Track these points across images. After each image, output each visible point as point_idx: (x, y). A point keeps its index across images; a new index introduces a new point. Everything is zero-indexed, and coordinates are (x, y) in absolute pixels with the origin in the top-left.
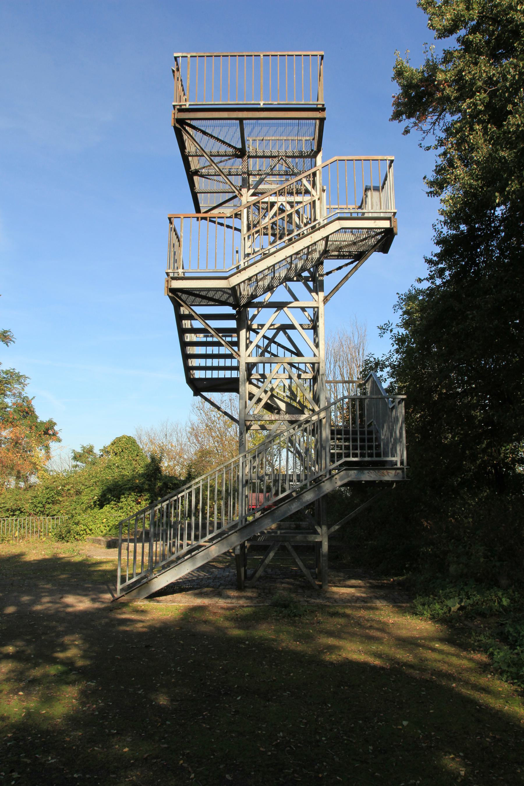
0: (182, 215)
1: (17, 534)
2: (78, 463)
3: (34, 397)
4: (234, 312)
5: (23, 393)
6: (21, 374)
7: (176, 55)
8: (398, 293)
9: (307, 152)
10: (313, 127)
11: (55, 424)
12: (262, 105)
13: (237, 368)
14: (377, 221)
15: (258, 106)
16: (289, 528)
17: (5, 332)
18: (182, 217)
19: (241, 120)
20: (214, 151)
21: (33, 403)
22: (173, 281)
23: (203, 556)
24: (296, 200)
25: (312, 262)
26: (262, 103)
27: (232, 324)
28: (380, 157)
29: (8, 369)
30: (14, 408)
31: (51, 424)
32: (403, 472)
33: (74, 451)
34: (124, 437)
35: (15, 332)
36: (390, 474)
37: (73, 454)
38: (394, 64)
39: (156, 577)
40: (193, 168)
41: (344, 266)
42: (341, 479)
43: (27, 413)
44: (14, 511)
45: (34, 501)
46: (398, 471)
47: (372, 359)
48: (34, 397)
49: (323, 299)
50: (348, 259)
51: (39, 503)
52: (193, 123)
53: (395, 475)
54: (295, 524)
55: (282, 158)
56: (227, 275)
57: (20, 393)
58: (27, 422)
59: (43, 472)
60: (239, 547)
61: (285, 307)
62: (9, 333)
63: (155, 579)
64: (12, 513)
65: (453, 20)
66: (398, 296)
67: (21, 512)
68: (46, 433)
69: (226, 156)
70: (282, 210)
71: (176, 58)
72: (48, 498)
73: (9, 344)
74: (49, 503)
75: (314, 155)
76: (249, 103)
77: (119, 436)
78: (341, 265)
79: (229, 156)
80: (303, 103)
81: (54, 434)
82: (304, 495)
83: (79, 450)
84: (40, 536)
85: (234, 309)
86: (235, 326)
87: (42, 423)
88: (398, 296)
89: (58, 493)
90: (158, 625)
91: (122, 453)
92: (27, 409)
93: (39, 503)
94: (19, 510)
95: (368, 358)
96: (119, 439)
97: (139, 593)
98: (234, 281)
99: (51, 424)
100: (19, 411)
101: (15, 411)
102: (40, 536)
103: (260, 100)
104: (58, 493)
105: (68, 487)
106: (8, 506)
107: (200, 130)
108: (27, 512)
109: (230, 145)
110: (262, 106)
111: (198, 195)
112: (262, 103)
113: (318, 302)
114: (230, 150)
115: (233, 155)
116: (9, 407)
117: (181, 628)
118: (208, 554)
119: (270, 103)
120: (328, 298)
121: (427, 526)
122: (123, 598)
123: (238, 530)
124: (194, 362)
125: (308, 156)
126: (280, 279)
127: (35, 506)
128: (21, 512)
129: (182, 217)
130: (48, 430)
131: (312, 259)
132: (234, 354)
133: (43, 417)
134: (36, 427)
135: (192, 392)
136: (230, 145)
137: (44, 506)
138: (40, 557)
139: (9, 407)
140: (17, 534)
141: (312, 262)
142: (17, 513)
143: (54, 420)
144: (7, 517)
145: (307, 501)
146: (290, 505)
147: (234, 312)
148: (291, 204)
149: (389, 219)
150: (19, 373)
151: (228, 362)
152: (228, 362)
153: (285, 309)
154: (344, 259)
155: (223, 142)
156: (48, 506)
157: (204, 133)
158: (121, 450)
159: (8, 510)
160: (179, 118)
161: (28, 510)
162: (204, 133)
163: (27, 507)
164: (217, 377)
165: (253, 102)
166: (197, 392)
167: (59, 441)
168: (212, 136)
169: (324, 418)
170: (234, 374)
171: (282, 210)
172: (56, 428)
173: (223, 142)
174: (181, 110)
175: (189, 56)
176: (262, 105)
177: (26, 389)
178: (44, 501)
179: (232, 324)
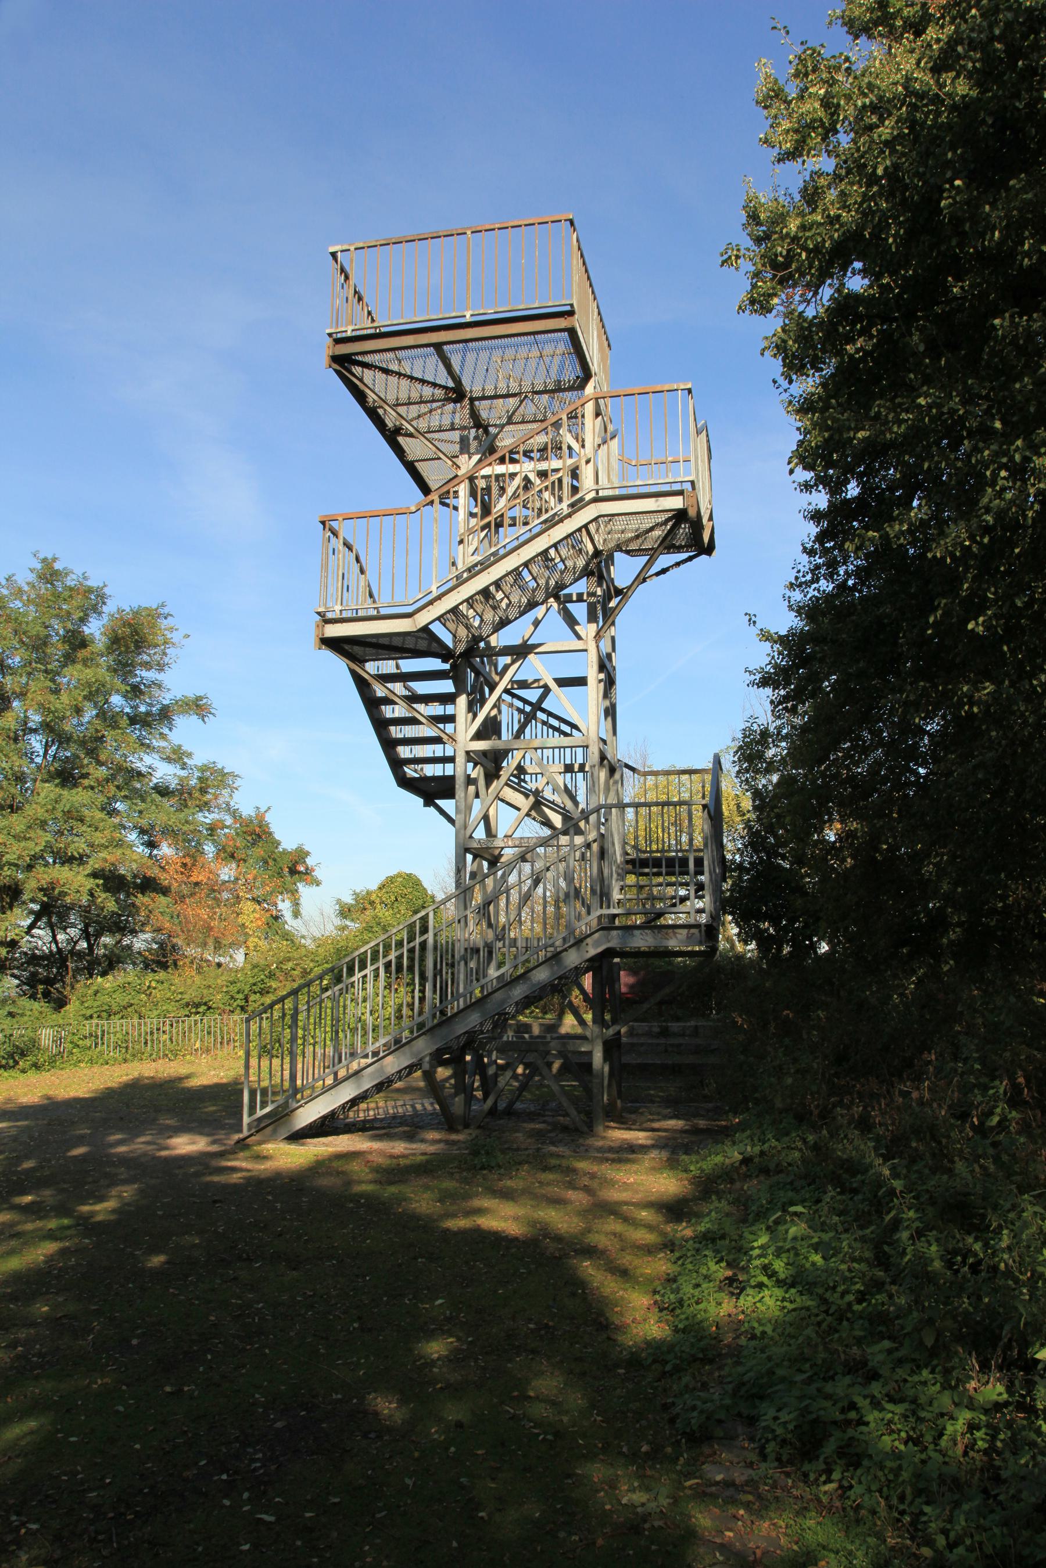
0: (341, 515)
1: (198, 1045)
2: (348, 923)
3: (269, 808)
4: (447, 666)
5: (232, 804)
6: (226, 771)
7: (332, 249)
8: (746, 614)
9: (569, 381)
10: (561, 345)
11: (308, 854)
12: (468, 316)
13: (451, 760)
14: (661, 499)
15: (463, 320)
16: (649, 1034)
17: (199, 698)
18: (340, 519)
19: (438, 347)
20: (403, 397)
21: (268, 818)
22: (327, 626)
23: (372, 1073)
24: (552, 467)
25: (574, 573)
26: (468, 314)
27: (446, 686)
28: (666, 387)
29: (205, 762)
30: (237, 829)
31: (301, 855)
32: (700, 931)
33: (339, 902)
34: (399, 875)
35: (215, 701)
36: (679, 936)
37: (337, 907)
38: (742, 202)
39: (301, 1106)
40: (390, 424)
41: (672, 566)
42: (597, 944)
43: (259, 836)
44: (197, 1006)
45: (231, 988)
46: (693, 931)
47: (755, 726)
48: (269, 808)
49: (594, 634)
50: (687, 551)
51: (238, 992)
52: (368, 359)
53: (688, 937)
54: (659, 1026)
55: (526, 397)
56: (409, 610)
57: (228, 804)
58: (259, 851)
59: (256, 940)
60: (427, 1059)
61: (530, 653)
62: (205, 701)
63: (301, 1110)
64: (194, 1010)
65: (796, 131)
66: (748, 617)
67: (209, 1008)
68: (293, 871)
69: (434, 401)
70: (527, 483)
71: (334, 255)
72: (254, 984)
73: (206, 719)
74: (255, 993)
75: (582, 387)
76: (447, 316)
77: (393, 872)
78: (665, 567)
79: (438, 401)
80: (536, 305)
81: (308, 872)
82: (534, 972)
83: (349, 899)
84: (235, 1047)
85: (445, 661)
86: (453, 690)
87: (285, 852)
88: (748, 617)
89: (271, 976)
90: (263, 1176)
91: (396, 904)
92: (257, 830)
93: (238, 992)
94: (205, 1004)
95: (749, 725)
96: (391, 880)
97: (275, 1131)
98: (423, 619)
99: (301, 855)
100: (245, 833)
101: (237, 834)
102: (235, 1047)
103: (467, 310)
104: (271, 976)
105: (289, 965)
106: (187, 998)
107: (376, 367)
108: (218, 1008)
109: (435, 385)
110: (468, 318)
111: (416, 464)
112: (468, 314)
113: (586, 642)
114: (439, 393)
115: (444, 400)
116: (227, 827)
117: (293, 1180)
118: (381, 1070)
119: (481, 312)
120: (601, 633)
121: (742, 1025)
122: (253, 1138)
123: (428, 1031)
124: (404, 752)
125: (571, 389)
126: (520, 607)
127: (232, 997)
128: (209, 1008)
129: (340, 519)
130: (296, 863)
131: (574, 568)
132: (445, 738)
133: (287, 840)
134: (275, 860)
135: (421, 801)
136: (435, 385)
137: (246, 999)
138: (215, 1080)
139: (227, 827)
140: (198, 1045)
141: (574, 573)
142: (202, 1009)
143: (306, 848)
144: (186, 1016)
145: (539, 983)
146: (510, 989)
147: (447, 666)
148: (543, 474)
149: (680, 493)
150: (223, 768)
151: (437, 750)
152: (437, 750)
153: (531, 657)
154: (679, 552)
155: (423, 381)
156: (252, 997)
157: (386, 371)
158: (393, 898)
159: (187, 1005)
160: (337, 353)
161: (221, 1006)
162: (386, 371)
163: (218, 999)
164: (441, 774)
165: (454, 314)
166: (429, 801)
167: (318, 884)
168: (399, 374)
169: (595, 841)
170: (449, 769)
171: (527, 483)
172: (310, 861)
173: (423, 381)
174: (338, 341)
175: (352, 248)
176: (468, 316)
177: (236, 795)
178: (247, 989)
179: (446, 686)
